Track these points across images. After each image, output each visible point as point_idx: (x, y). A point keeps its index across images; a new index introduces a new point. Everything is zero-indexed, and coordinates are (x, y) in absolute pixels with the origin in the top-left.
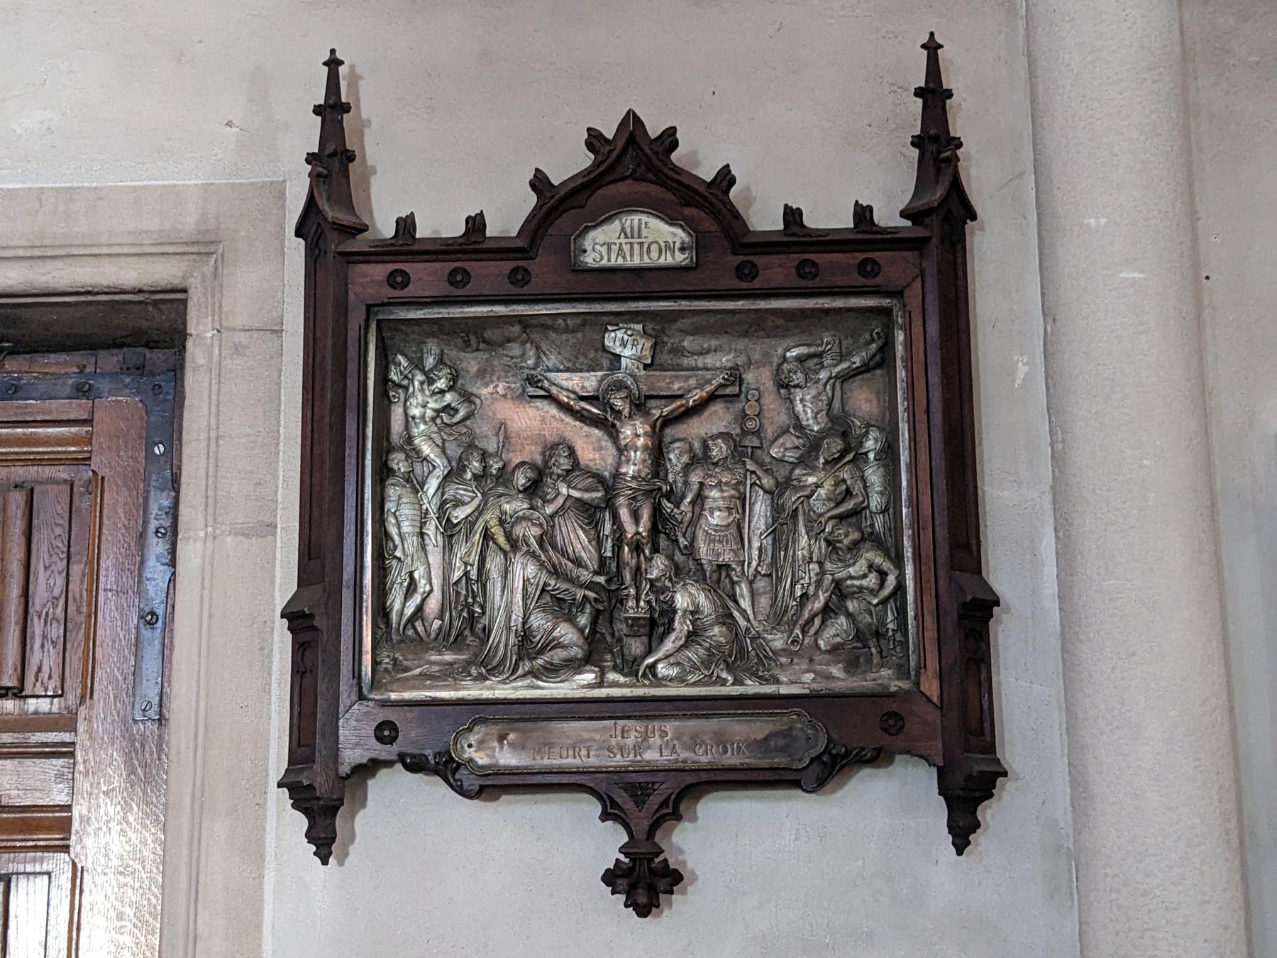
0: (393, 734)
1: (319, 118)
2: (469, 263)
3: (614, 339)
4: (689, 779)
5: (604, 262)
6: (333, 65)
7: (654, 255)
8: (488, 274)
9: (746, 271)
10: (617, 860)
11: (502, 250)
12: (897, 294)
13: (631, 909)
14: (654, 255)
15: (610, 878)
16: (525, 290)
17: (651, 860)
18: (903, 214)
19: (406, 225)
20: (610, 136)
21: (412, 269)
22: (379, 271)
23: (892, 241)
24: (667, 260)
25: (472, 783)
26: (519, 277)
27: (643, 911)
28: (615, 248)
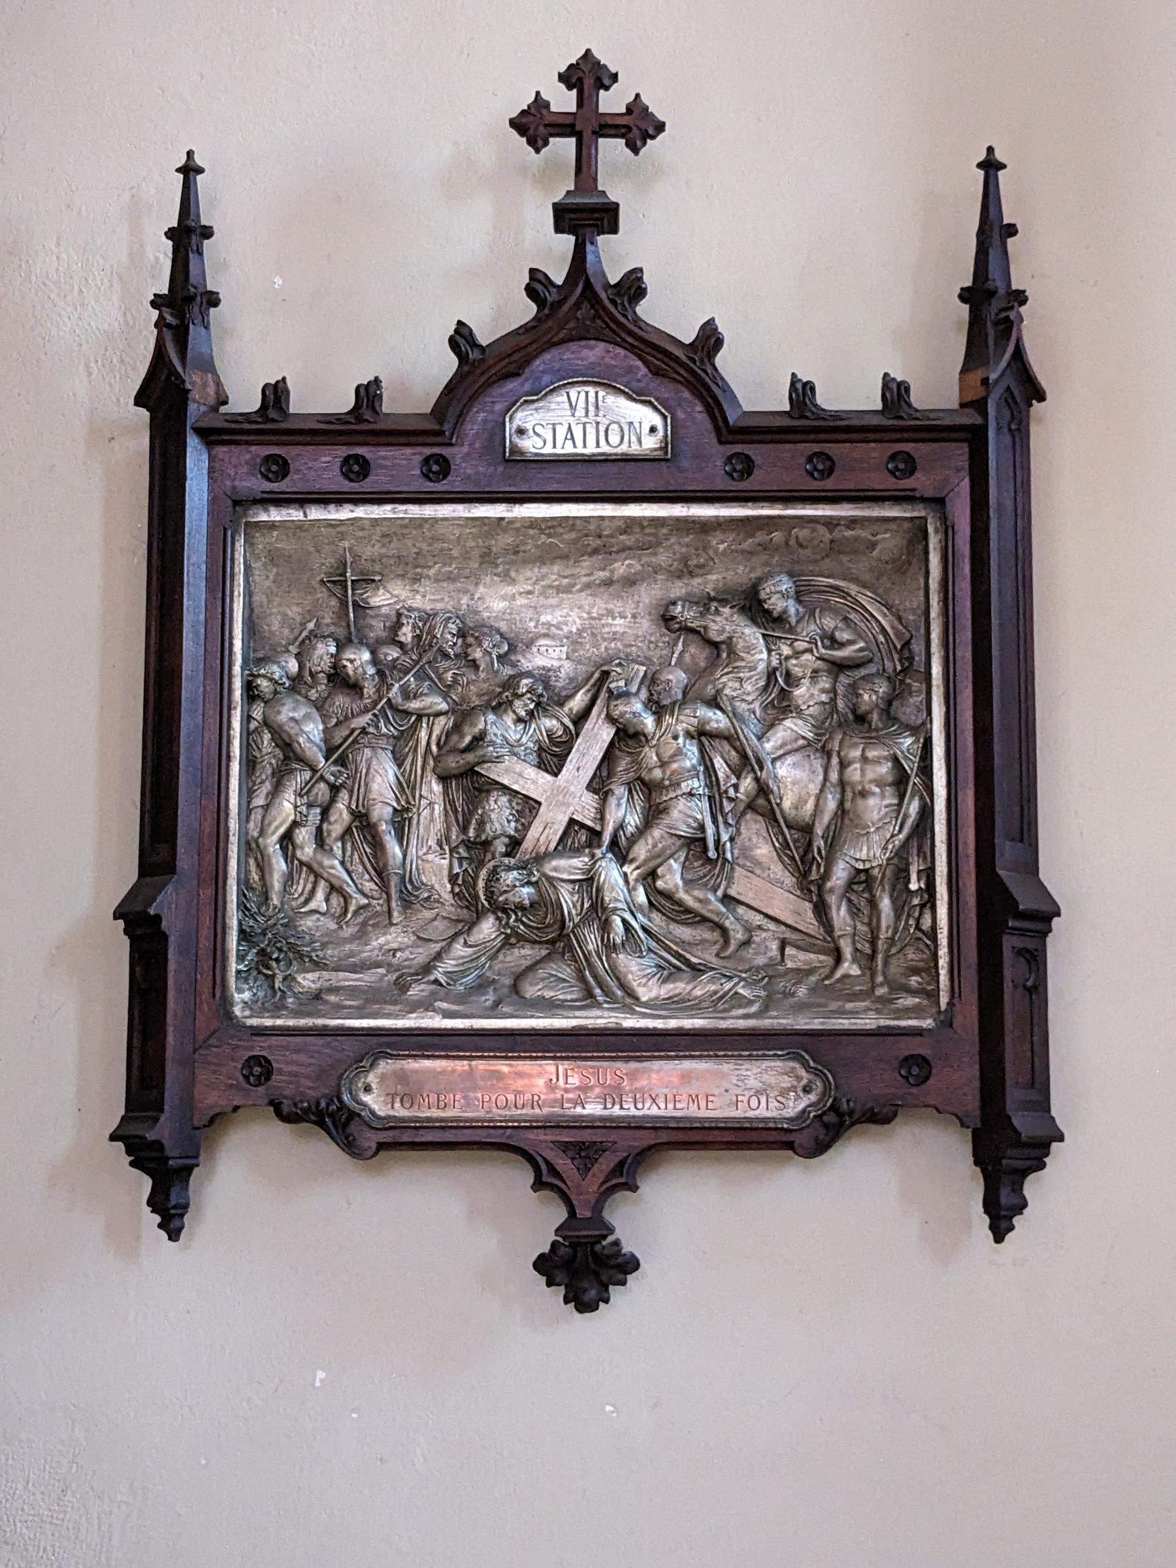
2: (912, 445)
4: (649, 1138)
5: (548, 450)
7: (614, 438)
14: (614, 438)
15: (542, 1265)
16: (829, 483)
17: (593, 1244)
19: (276, 394)
22: (876, 452)
25: (370, 1140)
26: (437, 467)
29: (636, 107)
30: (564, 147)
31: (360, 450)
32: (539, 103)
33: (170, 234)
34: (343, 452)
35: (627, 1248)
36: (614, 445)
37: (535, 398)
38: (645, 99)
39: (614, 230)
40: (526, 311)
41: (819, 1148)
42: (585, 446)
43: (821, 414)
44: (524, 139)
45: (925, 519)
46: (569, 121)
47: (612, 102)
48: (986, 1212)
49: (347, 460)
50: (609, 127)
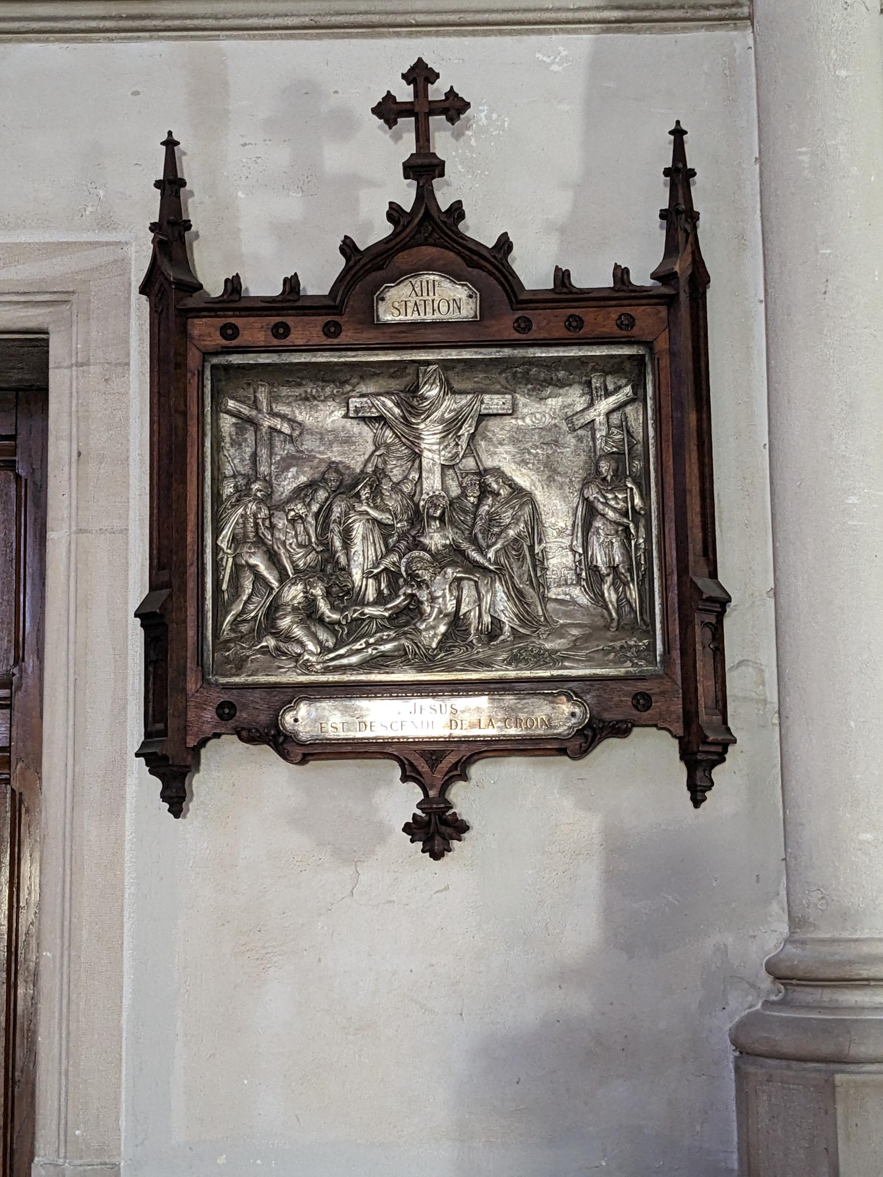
0: (225, 717)
1: (159, 191)
4: (475, 748)
6: (170, 145)
9: (523, 325)
10: (414, 815)
13: (428, 854)
14: (444, 309)
18: (654, 276)
19: (233, 285)
20: (408, 210)
21: (637, 312)
23: (641, 295)
27: (436, 856)
28: (410, 305)
29: (451, 94)
30: (407, 124)
31: (577, 312)
32: (389, 97)
36: (445, 314)
37: (392, 285)
38: (456, 90)
39: (442, 175)
41: (581, 753)
42: (425, 314)
44: (382, 120)
45: (214, 367)
46: (409, 107)
47: (437, 91)
48: (689, 789)
50: (436, 109)
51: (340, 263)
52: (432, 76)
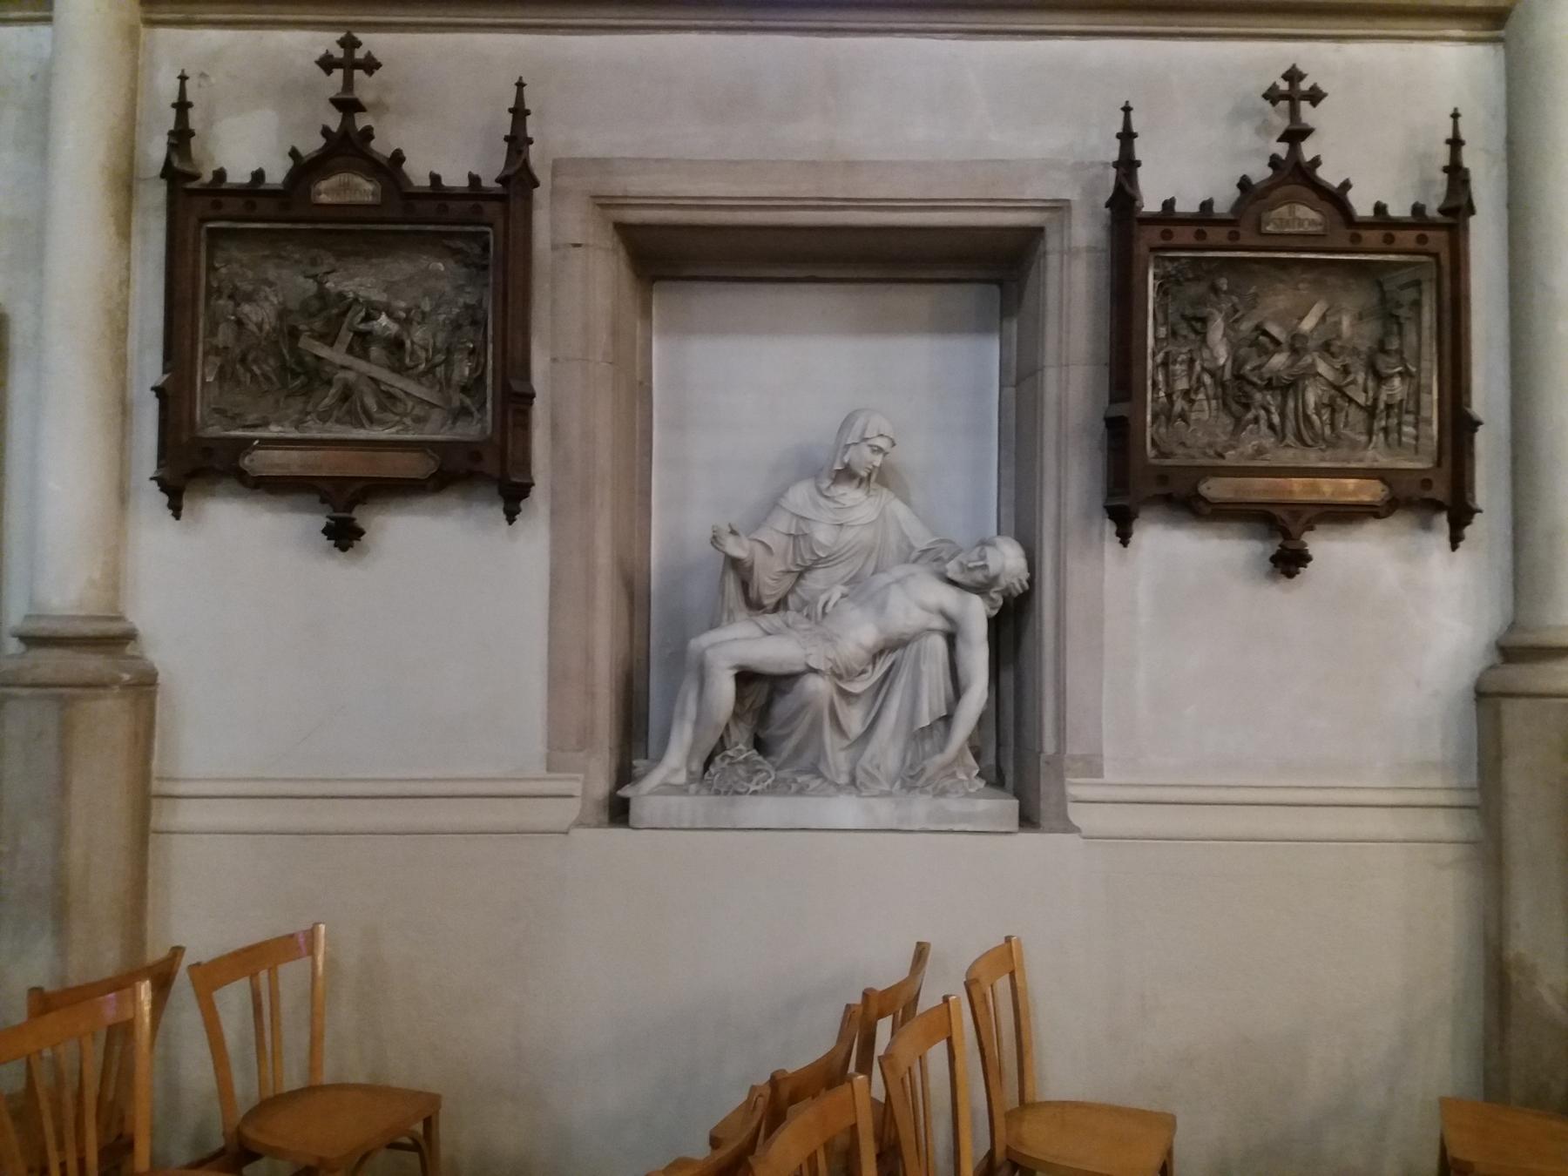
3: (288, 248)
8: (1217, 235)
11: (273, 193)
12: (490, 225)
18: (497, 181)
22: (1192, 230)
23: (490, 196)
24: (1312, 229)
26: (1234, 236)
30: (1284, 105)
33: (1119, 136)
34: (1162, 228)
35: (1310, 553)
40: (321, 142)
43: (1389, 218)
45: (210, 230)
47: (1305, 86)
49: (1231, 233)
50: (359, 65)
51: (1236, 193)
52: (1302, 77)
